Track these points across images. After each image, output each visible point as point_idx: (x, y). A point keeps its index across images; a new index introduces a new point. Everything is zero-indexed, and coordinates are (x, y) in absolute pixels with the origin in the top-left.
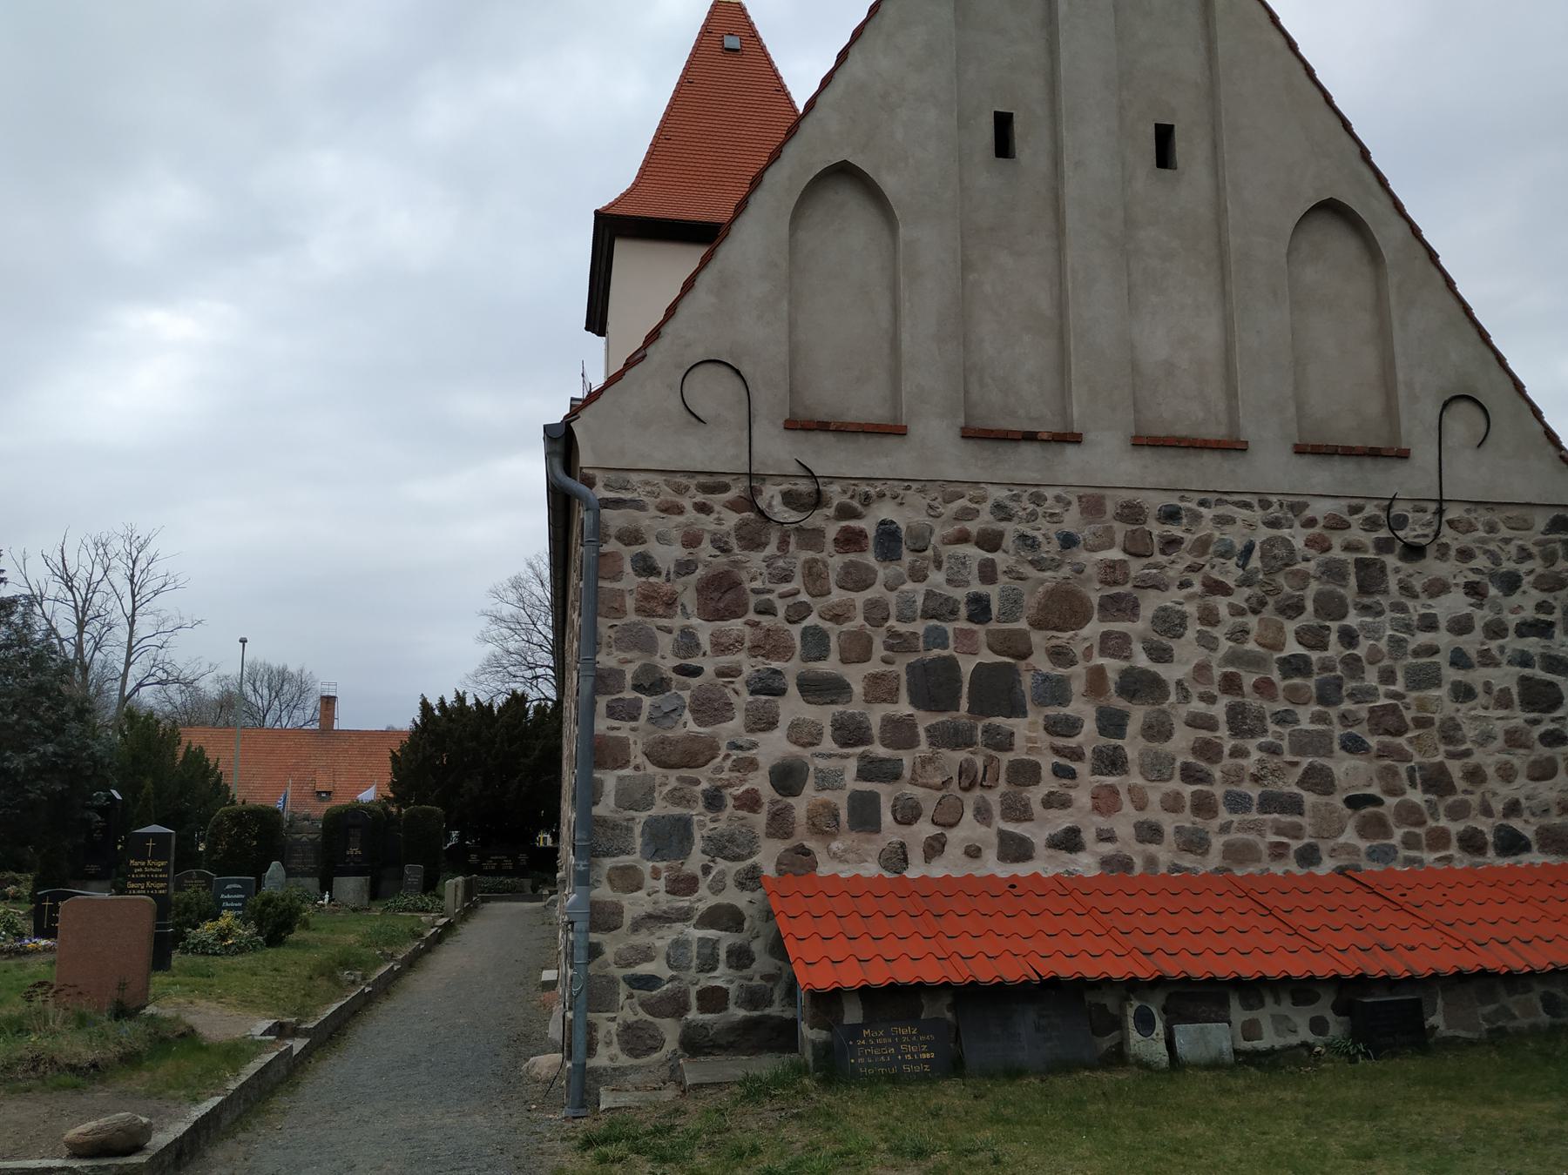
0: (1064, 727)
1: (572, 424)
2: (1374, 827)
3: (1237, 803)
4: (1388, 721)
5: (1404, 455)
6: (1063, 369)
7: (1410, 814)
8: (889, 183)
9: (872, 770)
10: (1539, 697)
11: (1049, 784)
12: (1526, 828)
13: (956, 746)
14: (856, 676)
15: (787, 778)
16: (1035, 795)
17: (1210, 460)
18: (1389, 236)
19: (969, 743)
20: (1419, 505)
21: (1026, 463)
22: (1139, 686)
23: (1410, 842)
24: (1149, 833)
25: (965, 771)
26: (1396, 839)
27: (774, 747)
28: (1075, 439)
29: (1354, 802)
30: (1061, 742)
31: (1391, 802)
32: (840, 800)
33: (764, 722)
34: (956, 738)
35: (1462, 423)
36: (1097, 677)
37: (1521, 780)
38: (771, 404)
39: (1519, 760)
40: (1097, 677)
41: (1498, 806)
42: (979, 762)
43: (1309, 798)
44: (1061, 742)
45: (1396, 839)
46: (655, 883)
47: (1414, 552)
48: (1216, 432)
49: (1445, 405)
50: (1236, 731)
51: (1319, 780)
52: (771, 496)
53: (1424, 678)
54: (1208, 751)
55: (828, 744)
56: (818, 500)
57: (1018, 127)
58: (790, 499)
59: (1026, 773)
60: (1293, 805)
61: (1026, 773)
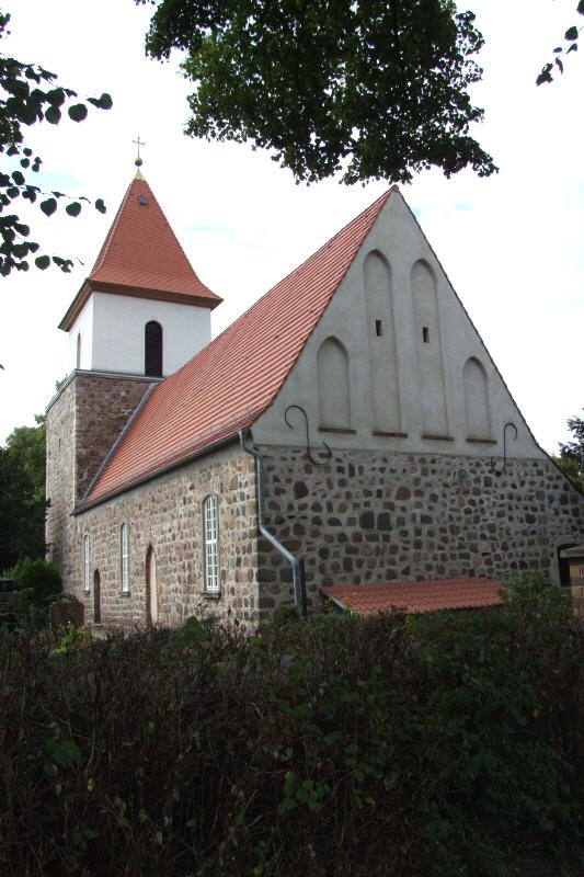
0: (404, 533)
1: (144, 373)
2: (488, 562)
3: (453, 557)
4: (492, 528)
5: (495, 442)
6: (399, 412)
7: (498, 557)
8: (347, 344)
9: (350, 550)
10: (576, 513)
11: (401, 552)
12: (526, 559)
13: (373, 541)
14: (343, 518)
15: (324, 553)
16: (397, 557)
17: (443, 443)
18: (489, 369)
19: (377, 539)
20: (499, 459)
21: (391, 445)
22: (425, 519)
23: (498, 566)
24: (429, 567)
25: (377, 549)
26: (494, 566)
27: (319, 543)
28: (405, 436)
29: (484, 554)
30: (404, 539)
31: (493, 554)
32: (340, 561)
33: (316, 534)
34: (374, 538)
35: (510, 433)
36: (414, 518)
37: (526, 546)
38: (314, 424)
39: (526, 539)
40: (414, 518)
41: (520, 554)
42: (381, 546)
43: (472, 554)
44: (404, 539)
45: (494, 566)
46: (359, 570)
47: (498, 474)
48: (443, 434)
49: (506, 426)
50: (453, 533)
51: (474, 549)
52: (315, 456)
53: (500, 515)
54: (445, 540)
55: (336, 542)
56: (329, 456)
57: (383, 326)
58: (321, 455)
59: (394, 549)
60: (466, 556)
61: (394, 549)
